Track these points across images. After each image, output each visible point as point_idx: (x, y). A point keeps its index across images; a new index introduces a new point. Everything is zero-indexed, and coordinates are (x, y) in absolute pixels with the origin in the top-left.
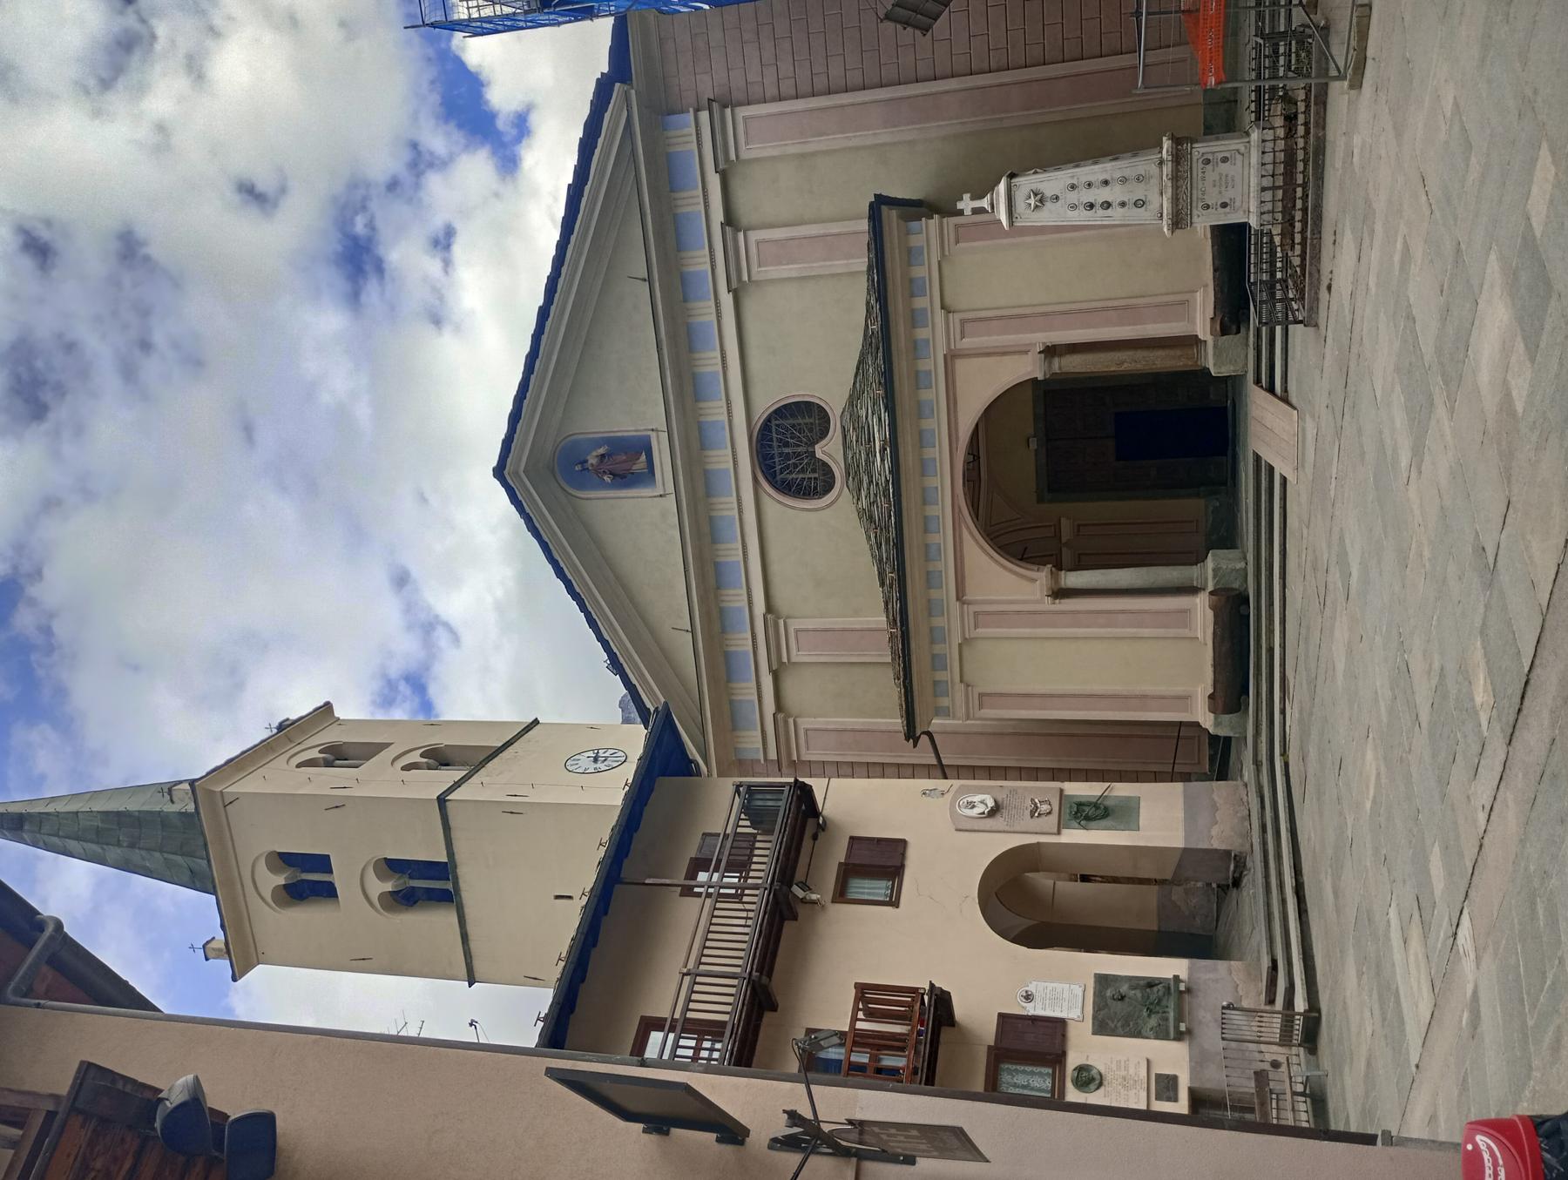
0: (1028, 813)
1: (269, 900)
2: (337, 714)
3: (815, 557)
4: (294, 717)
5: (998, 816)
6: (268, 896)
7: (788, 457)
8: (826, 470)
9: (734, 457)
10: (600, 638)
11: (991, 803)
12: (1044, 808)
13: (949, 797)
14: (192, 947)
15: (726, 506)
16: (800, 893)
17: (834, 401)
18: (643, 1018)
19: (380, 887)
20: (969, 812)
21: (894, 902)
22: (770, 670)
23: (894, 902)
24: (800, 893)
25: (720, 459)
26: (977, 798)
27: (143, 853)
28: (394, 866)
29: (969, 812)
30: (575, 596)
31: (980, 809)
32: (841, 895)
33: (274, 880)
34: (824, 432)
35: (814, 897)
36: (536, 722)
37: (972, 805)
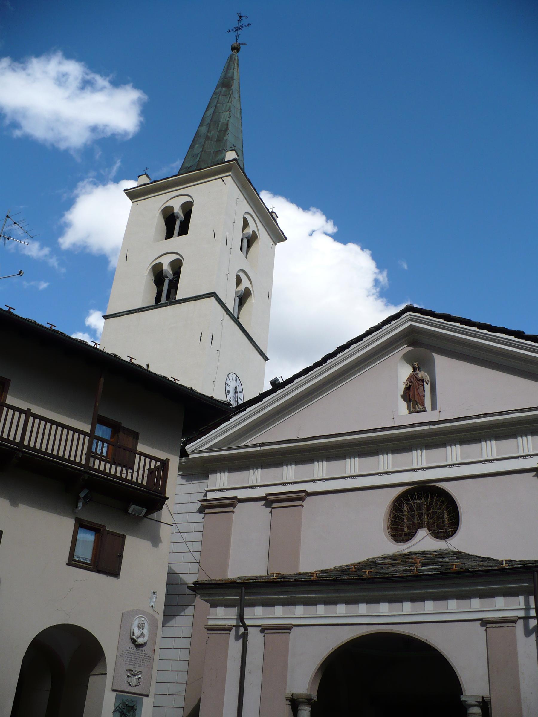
0: (131, 668)
1: (167, 204)
2: (278, 244)
3: (349, 527)
4: (278, 220)
5: (132, 645)
6: (170, 204)
7: (420, 509)
8: (408, 536)
9: (421, 466)
10: (296, 377)
11: (140, 641)
12: (134, 681)
13: (151, 611)
14: (147, 169)
15: (386, 461)
16: (82, 495)
17: (456, 543)
18: (9, 381)
19: (166, 262)
20: (136, 623)
21: (72, 562)
22: (267, 495)
23: (72, 562)
24: (82, 495)
25: (419, 458)
26: (145, 631)
27: (203, 143)
28: (177, 266)
29: (136, 623)
30: (325, 360)
31: (137, 632)
32: (81, 525)
33: (177, 205)
34: (437, 536)
35: (80, 505)
36: (266, 359)
37: (141, 627)
